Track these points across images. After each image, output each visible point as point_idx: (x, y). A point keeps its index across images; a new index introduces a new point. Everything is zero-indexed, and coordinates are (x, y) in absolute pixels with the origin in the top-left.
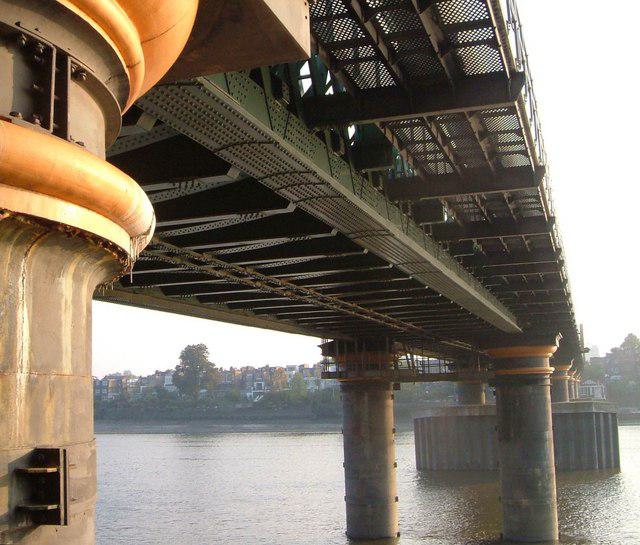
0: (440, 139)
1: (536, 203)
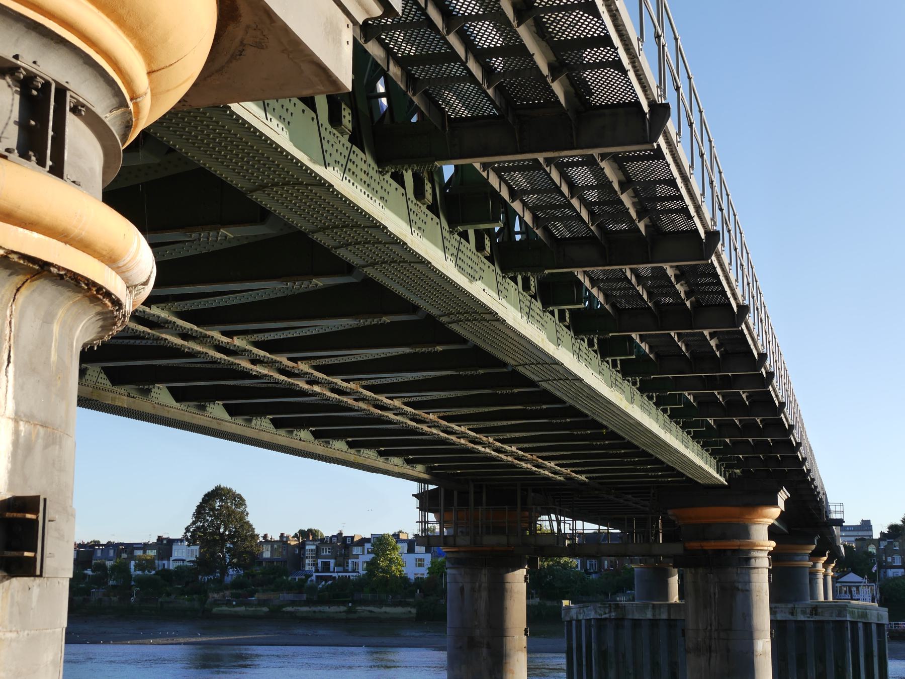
0: (565, 189)
1: (713, 284)
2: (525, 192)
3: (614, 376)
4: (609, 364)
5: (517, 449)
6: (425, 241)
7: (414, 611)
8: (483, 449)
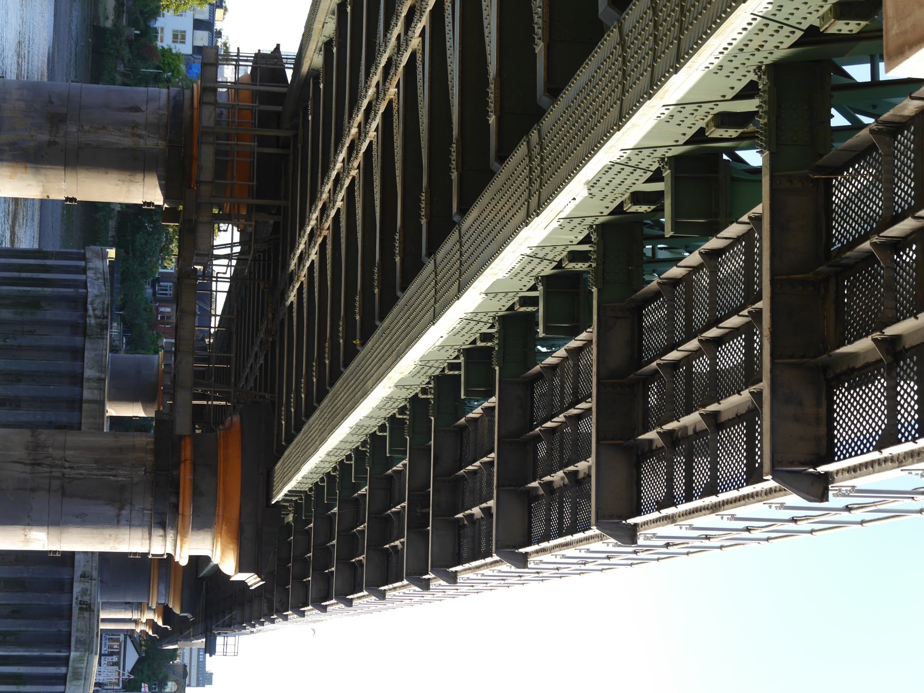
0: (713, 332)
1: (561, 523)
2: (714, 272)
3: (436, 365)
4: (455, 358)
5: (339, 209)
6: (652, 123)
7: (109, 24)
8: (340, 158)
